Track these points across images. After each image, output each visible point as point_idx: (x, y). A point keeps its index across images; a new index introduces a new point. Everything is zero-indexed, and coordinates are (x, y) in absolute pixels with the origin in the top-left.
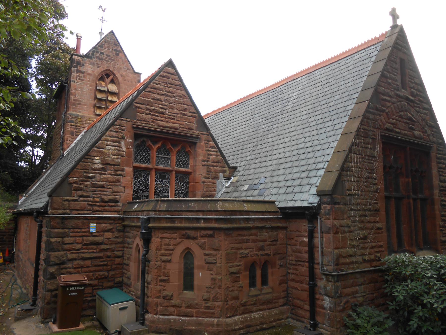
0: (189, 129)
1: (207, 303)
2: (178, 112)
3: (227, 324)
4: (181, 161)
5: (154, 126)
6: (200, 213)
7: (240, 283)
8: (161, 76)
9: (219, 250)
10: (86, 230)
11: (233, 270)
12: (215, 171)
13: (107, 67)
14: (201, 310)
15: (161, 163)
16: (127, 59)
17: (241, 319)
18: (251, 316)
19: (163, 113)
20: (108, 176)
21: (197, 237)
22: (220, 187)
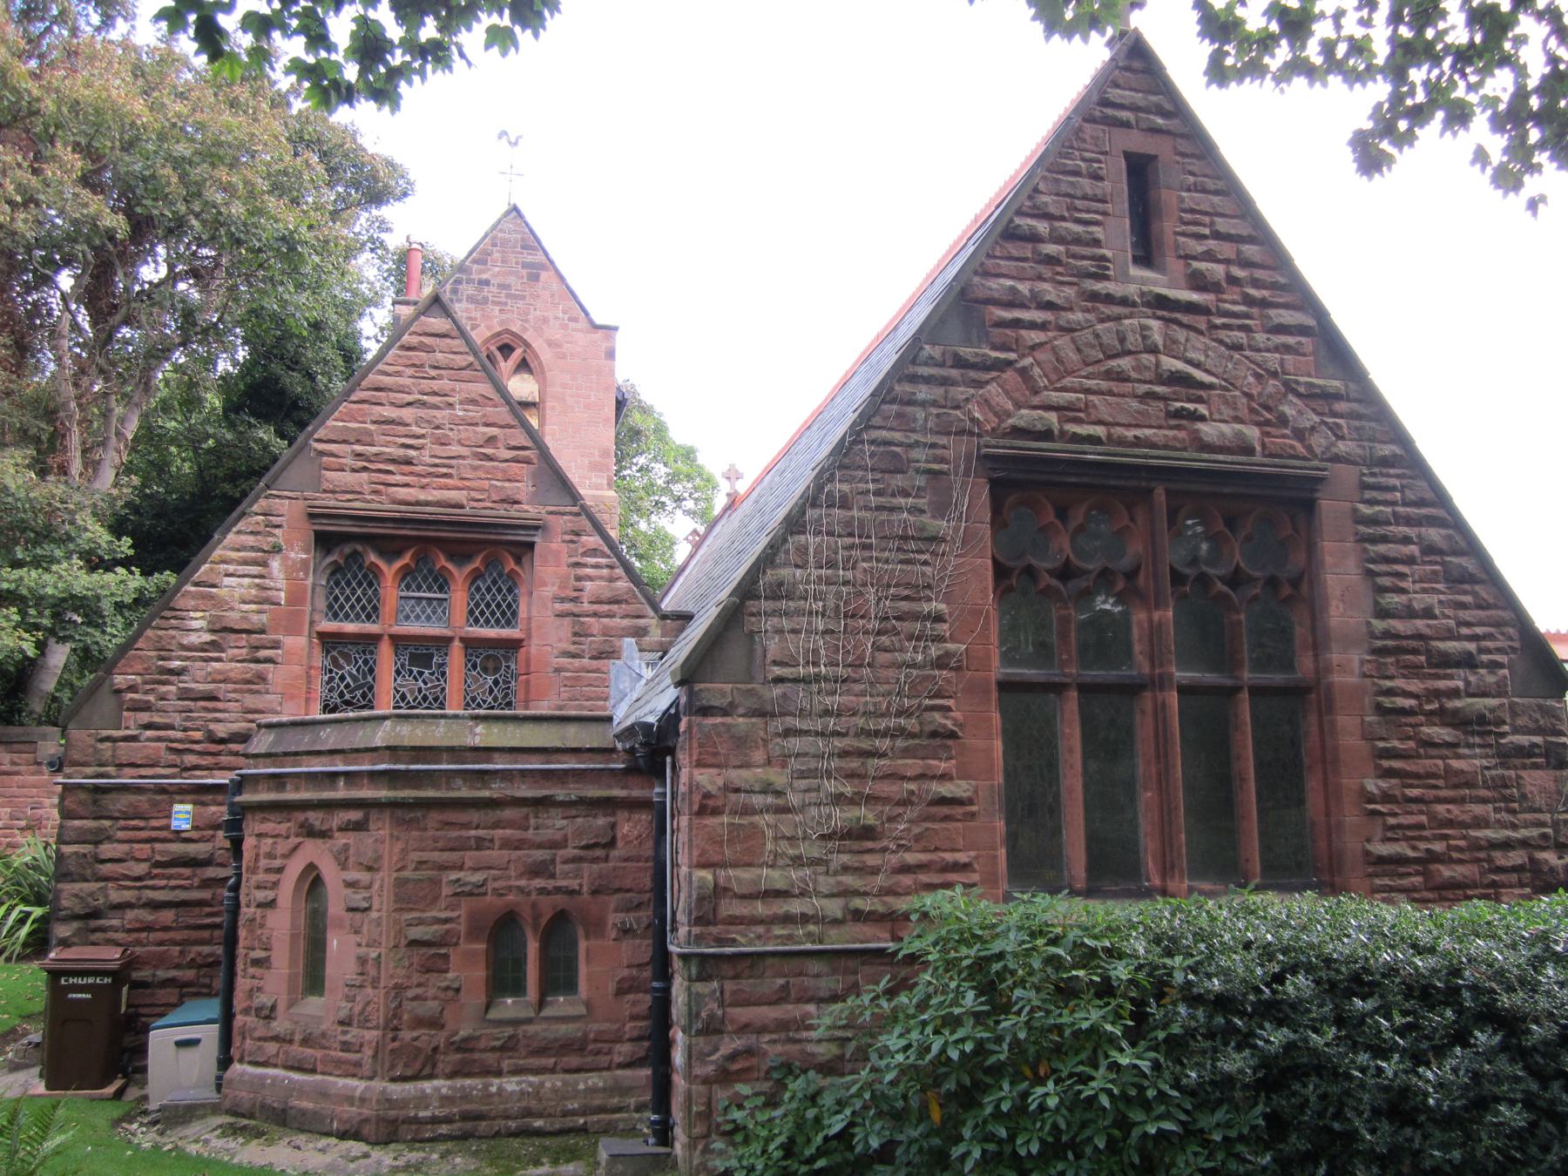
0: (503, 501)
1: (345, 1033)
3: (388, 1100)
4: (488, 605)
5: (381, 505)
6: (338, 757)
7: (450, 975)
8: (403, 348)
9: (378, 870)
10: (163, 822)
11: (417, 933)
12: (606, 632)
14: (332, 1053)
15: (418, 617)
16: (568, 288)
17: (444, 1091)
18: (486, 1087)
19: (409, 462)
20: (230, 664)
21: (331, 830)
22: (625, 684)
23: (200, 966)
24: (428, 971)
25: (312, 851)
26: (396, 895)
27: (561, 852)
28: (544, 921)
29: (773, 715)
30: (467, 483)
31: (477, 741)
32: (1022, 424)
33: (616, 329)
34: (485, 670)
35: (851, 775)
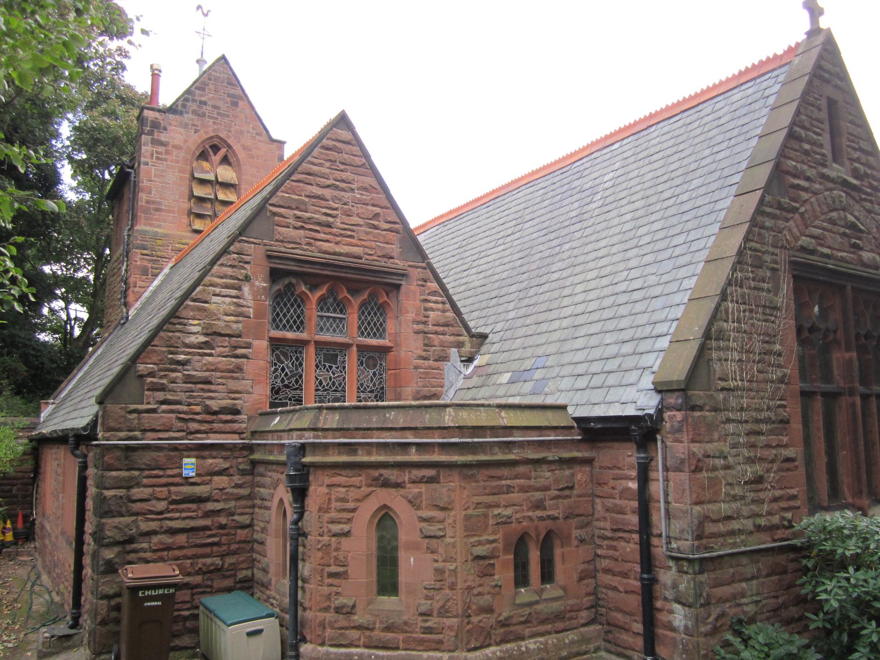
0: (383, 256)
2: (361, 221)
4: (369, 324)
6: (408, 433)
7: (496, 577)
8: (323, 147)
10: (176, 471)
11: (480, 550)
12: (442, 344)
13: (214, 131)
17: (498, 653)
18: (519, 647)
19: (329, 226)
20: (218, 358)
21: (404, 482)
23: (205, 573)
24: (485, 575)
25: (383, 496)
26: (465, 526)
27: (549, 493)
28: (542, 537)
29: (721, 411)
30: (363, 243)
31: (505, 422)
32: (804, 245)
33: (284, 143)
34: (368, 366)
35: (753, 446)
